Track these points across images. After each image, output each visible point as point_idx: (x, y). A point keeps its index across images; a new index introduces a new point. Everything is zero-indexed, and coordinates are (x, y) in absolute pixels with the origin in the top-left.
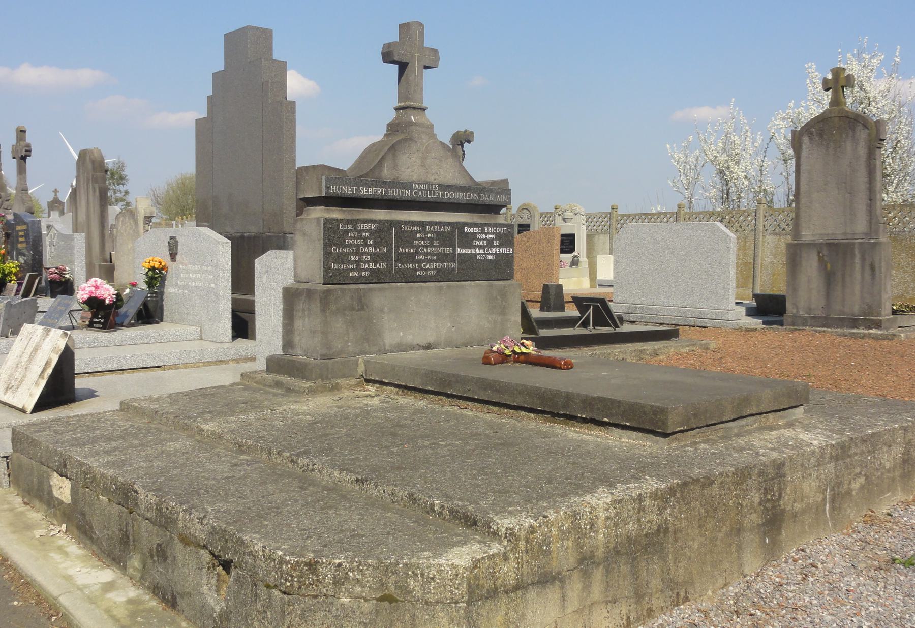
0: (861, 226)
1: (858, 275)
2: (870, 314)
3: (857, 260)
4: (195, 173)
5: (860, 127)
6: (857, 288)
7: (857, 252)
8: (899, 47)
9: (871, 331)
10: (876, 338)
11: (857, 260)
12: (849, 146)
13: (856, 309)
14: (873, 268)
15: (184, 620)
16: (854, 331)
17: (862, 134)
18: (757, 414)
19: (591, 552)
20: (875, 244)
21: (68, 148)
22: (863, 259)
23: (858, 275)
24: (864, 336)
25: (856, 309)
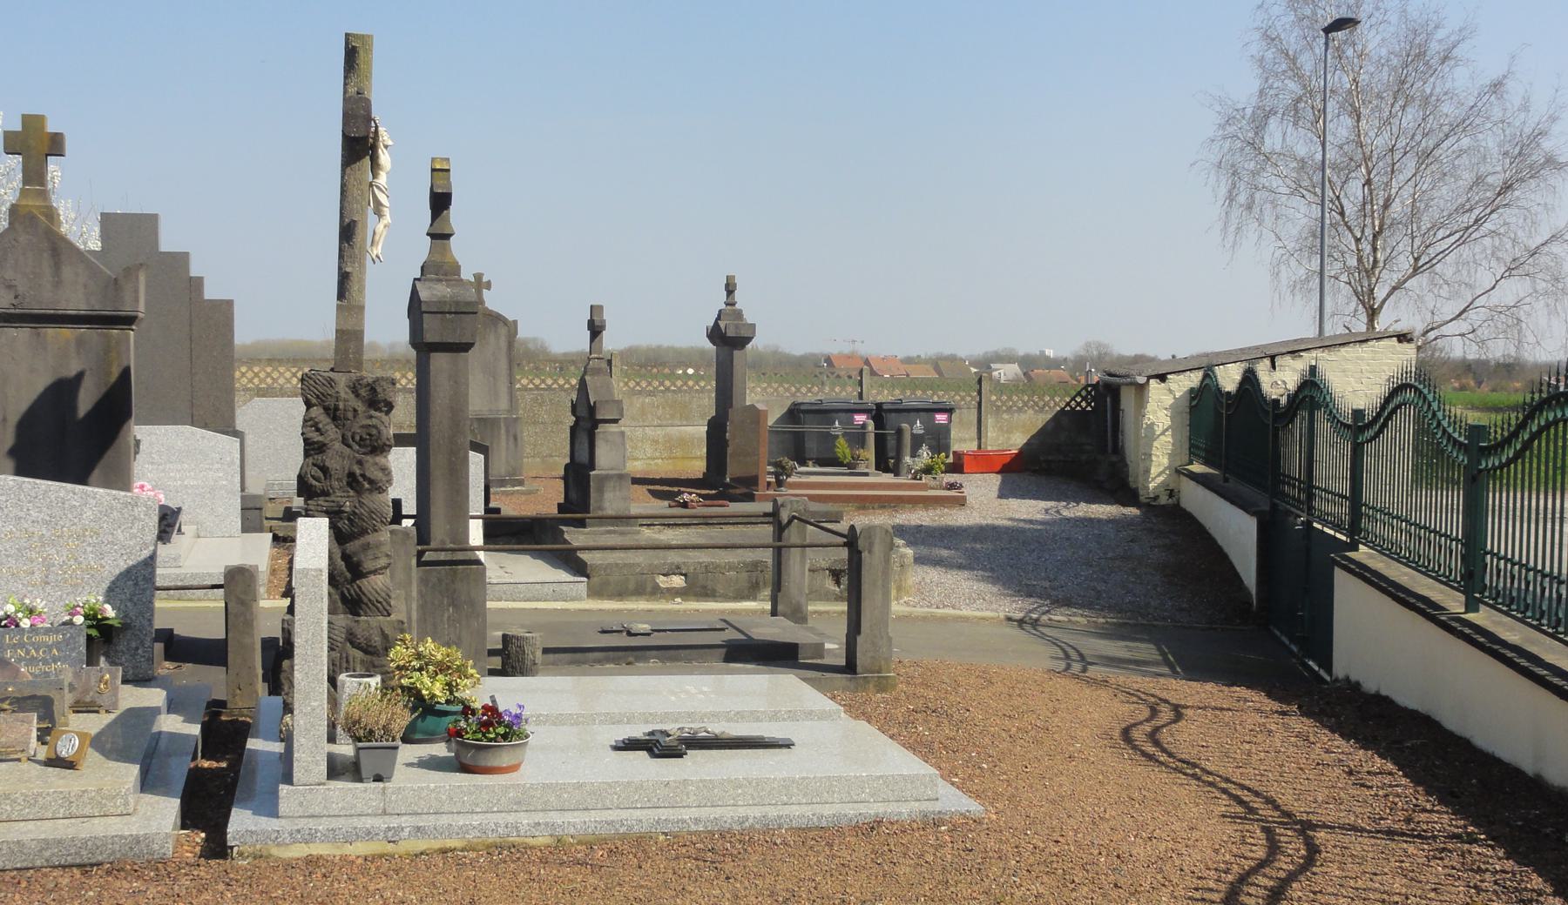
0: (504, 404)
1: (503, 443)
2: (514, 475)
3: (503, 431)
4: (238, 412)
5: (501, 324)
6: (504, 454)
7: (502, 425)
8: (224, 765)
9: (516, 488)
10: (523, 493)
11: (503, 431)
12: (492, 338)
13: (503, 471)
14: (515, 438)
15: (1538, 145)
16: (503, 489)
17: (503, 331)
18: (251, 509)
19: (385, 444)
20: (517, 419)
21: (135, 341)
22: (507, 431)
23: (503, 443)
24: (513, 493)
25: (503, 471)
